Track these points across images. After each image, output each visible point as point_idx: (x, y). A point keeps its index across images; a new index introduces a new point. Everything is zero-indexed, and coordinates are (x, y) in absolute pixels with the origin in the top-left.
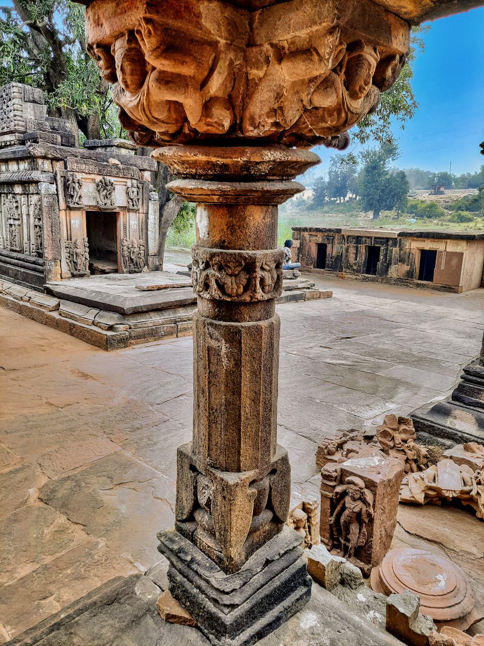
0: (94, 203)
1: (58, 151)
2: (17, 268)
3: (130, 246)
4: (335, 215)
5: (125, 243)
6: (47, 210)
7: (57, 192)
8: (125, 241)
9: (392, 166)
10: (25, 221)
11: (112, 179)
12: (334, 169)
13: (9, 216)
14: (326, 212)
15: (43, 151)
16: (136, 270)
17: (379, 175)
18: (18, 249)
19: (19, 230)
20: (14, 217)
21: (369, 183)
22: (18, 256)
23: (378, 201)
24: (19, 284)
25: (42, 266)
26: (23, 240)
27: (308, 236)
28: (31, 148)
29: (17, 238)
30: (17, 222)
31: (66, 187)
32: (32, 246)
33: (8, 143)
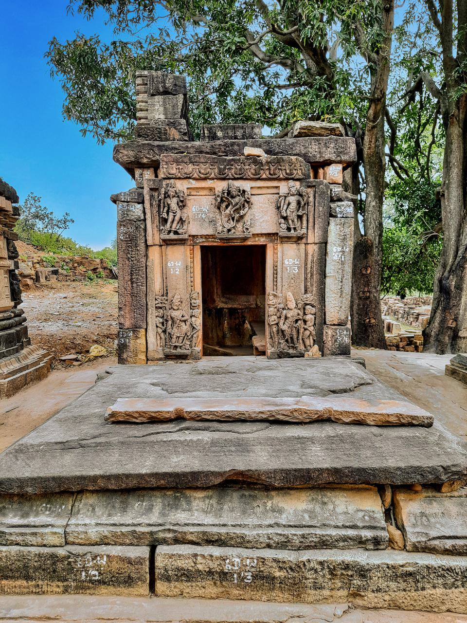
0: (209, 231)
11: (246, 185)
16: (291, 351)
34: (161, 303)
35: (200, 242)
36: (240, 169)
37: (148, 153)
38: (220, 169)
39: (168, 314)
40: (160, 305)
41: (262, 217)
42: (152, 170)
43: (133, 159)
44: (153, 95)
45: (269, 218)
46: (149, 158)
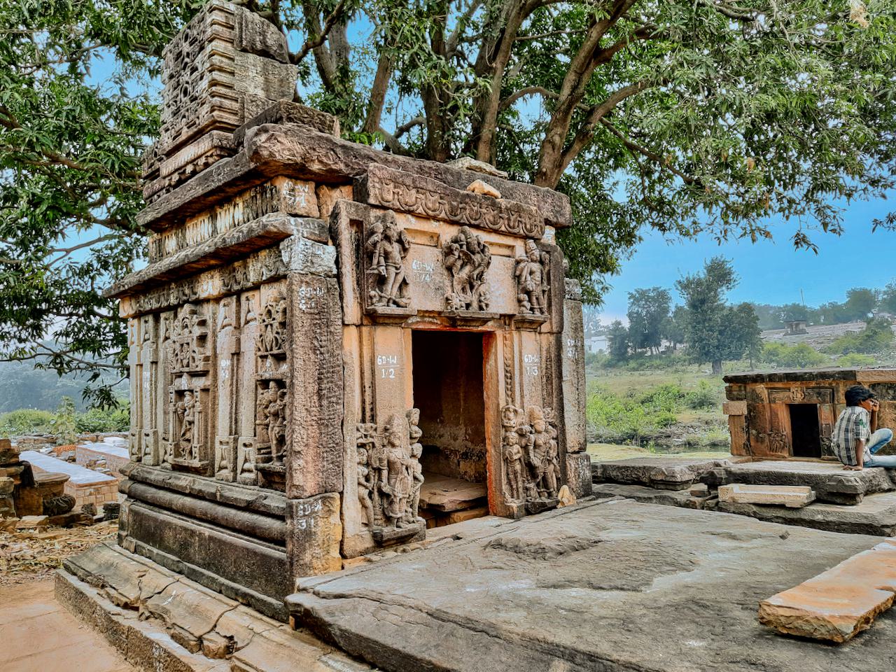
0: (437, 305)
1: (339, 150)
2: (190, 524)
3: (527, 428)
4: (649, 373)
5: (514, 421)
6: (307, 323)
7: (338, 268)
8: (511, 415)
9: (729, 298)
10: (224, 375)
11: (484, 237)
12: (636, 309)
13: (178, 368)
14: (634, 369)
15: (299, 149)
17: (713, 311)
18: (196, 463)
19: (204, 404)
20: (192, 368)
21: (699, 323)
22: (197, 487)
23: (717, 347)
24: (193, 576)
25: (281, 518)
26: (213, 434)
27: (766, 391)
28: (264, 137)
29: (195, 429)
30: (199, 383)
31: (364, 254)
32: (242, 452)
33: (189, 169)
34: (366, 436)
35: (413, 323)
36: (477, 213)
37: (326, 156)
38: (452, 207)
39: (384, 456)
40: (363, 441)
41: (497, 289)
42: (313, 185)
43: (299, 160)
44: (244, 50)
45: (506, 291)
46: (326, 165)
